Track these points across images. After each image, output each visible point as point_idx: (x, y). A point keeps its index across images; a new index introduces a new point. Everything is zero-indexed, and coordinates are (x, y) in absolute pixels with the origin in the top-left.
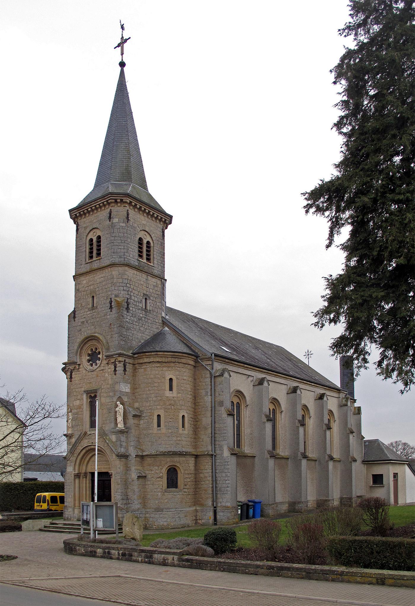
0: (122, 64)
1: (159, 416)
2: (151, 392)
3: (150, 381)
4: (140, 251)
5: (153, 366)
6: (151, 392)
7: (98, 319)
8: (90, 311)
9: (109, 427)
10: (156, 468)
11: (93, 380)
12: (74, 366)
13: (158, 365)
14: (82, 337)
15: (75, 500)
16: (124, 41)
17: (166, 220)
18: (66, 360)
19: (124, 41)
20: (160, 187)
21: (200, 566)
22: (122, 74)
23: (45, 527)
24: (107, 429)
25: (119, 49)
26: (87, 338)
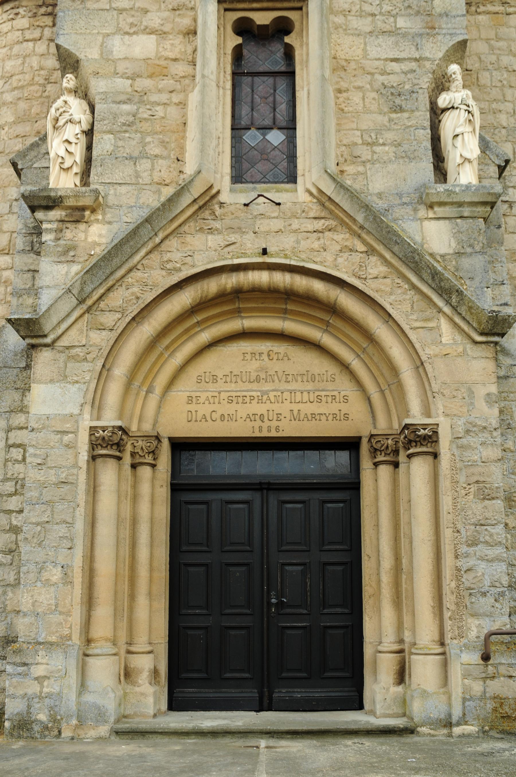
9: (391, 177)
15: (90, 601)
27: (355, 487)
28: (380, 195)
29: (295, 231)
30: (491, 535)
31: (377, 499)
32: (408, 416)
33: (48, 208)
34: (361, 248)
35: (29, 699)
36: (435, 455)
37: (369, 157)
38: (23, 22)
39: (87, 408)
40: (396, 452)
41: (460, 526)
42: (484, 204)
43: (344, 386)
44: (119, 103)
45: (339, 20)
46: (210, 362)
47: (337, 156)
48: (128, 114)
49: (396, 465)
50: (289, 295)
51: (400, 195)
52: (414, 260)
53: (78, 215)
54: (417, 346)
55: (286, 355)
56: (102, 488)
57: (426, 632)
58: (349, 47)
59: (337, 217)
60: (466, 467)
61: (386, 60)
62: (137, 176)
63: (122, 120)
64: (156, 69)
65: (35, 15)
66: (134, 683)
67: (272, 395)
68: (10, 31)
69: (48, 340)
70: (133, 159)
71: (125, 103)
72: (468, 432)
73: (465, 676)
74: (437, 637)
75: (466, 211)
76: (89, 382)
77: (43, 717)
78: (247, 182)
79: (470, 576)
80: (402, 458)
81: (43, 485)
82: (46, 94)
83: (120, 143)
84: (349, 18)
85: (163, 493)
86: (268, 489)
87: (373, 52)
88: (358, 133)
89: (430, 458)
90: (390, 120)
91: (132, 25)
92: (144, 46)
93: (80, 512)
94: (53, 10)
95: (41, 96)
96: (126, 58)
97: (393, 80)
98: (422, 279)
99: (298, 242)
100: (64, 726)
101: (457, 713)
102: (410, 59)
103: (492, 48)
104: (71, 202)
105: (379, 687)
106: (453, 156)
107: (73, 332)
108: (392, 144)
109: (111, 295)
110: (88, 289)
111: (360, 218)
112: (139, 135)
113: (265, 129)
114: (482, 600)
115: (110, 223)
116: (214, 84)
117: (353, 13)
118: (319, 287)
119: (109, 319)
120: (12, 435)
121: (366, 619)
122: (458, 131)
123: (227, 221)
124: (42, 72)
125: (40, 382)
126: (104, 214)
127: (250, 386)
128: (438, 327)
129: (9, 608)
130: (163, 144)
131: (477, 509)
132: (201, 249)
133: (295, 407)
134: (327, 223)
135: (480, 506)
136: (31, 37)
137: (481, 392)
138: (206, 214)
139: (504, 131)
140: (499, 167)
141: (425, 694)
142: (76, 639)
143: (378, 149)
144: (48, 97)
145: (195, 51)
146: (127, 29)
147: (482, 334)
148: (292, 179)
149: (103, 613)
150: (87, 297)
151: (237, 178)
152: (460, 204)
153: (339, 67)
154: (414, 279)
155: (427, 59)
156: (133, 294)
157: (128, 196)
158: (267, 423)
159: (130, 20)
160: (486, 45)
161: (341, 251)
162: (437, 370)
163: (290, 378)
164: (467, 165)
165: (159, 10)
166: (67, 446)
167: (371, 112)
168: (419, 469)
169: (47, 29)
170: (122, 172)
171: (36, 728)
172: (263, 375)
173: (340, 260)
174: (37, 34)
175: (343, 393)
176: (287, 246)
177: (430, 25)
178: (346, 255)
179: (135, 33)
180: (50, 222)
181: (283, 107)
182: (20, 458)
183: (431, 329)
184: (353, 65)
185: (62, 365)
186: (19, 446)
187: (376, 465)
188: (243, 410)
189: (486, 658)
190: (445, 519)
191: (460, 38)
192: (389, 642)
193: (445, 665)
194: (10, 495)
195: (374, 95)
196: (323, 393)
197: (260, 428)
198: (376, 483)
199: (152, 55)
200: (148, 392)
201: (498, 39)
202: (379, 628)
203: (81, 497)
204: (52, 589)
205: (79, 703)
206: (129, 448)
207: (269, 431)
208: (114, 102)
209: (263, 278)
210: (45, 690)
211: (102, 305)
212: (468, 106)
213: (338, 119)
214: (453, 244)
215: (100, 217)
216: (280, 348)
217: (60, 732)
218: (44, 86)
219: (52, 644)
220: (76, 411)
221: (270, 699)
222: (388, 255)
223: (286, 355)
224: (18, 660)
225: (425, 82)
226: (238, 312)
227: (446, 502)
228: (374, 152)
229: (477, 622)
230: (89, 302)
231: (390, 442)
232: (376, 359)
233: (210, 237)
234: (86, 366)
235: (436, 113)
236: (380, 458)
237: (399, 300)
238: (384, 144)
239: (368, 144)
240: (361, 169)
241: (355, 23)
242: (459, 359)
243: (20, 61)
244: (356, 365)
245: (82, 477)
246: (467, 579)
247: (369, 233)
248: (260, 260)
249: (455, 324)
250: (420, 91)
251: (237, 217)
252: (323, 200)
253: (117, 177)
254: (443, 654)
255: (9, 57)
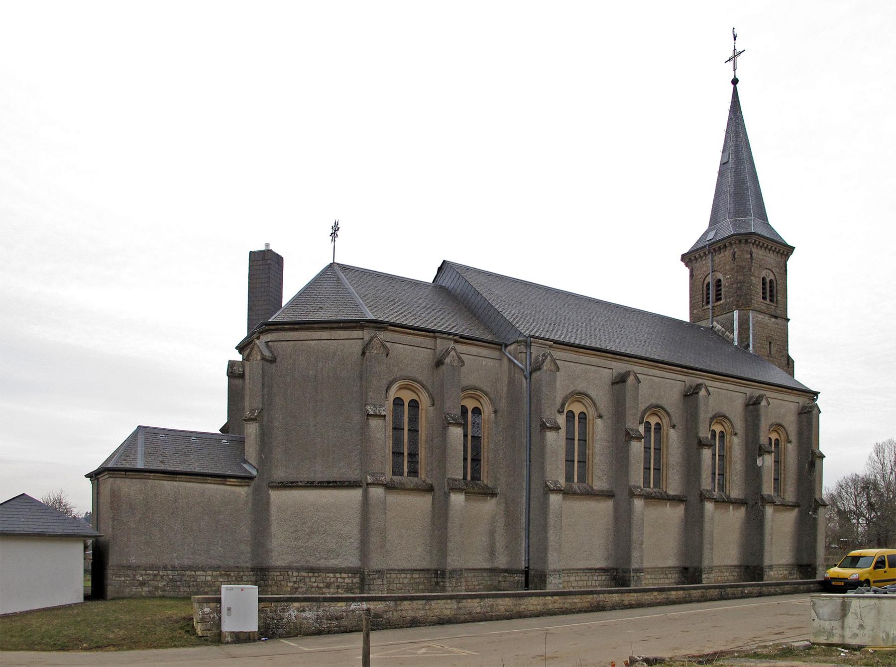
0: (735, 82)
4: (763, 293)
16: (736, 55)
17: (787, 251)
19: (736, 55)
20: (782, 219)
21: (599, 608)
22: (735, 91)
25: (731, 63)
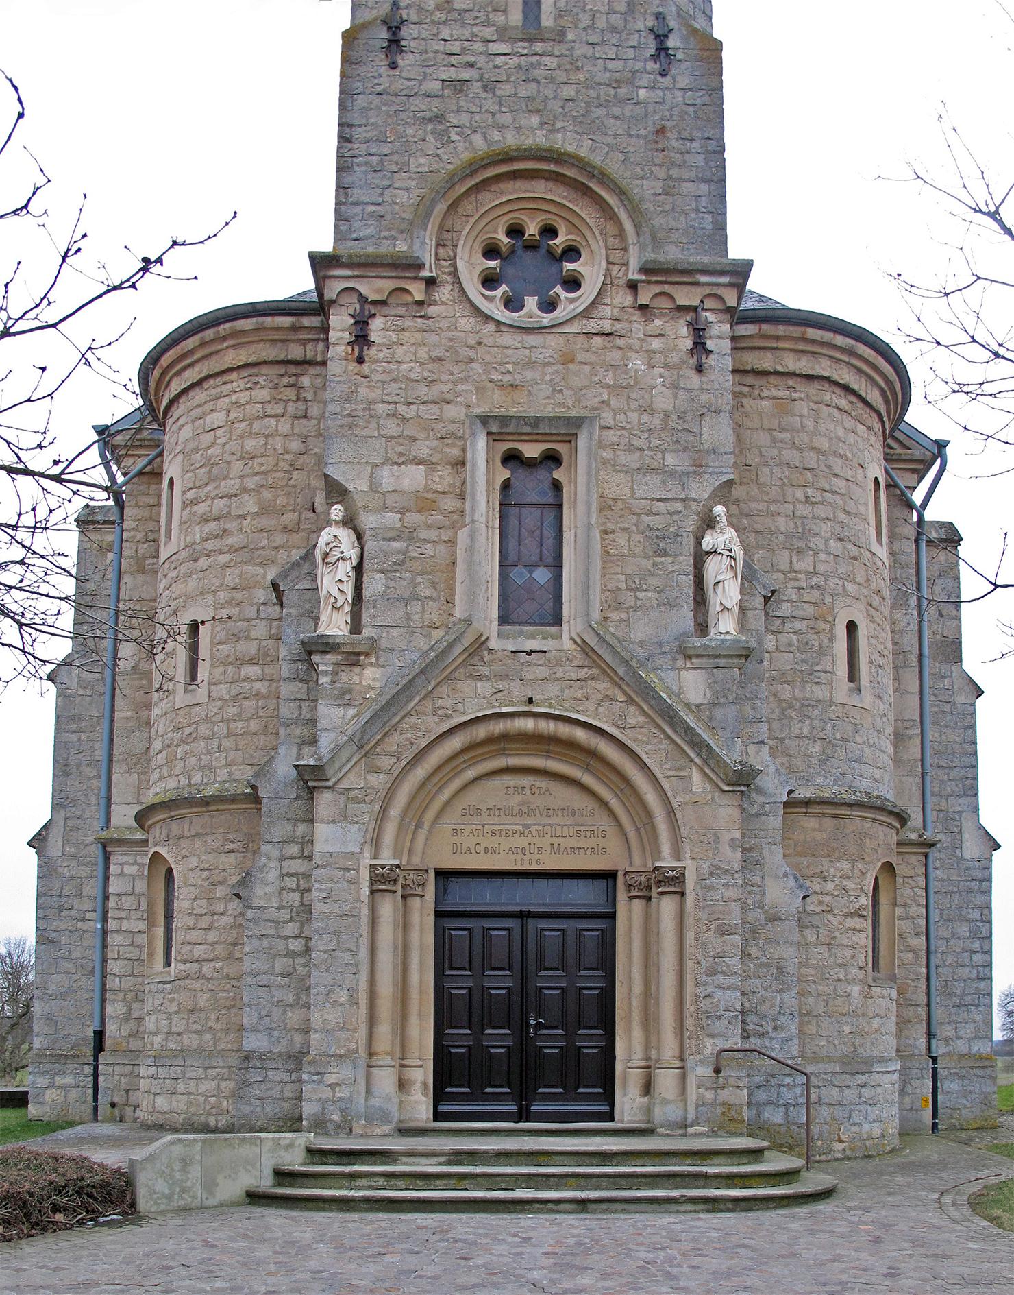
1: (851, 627)
2: (821, 511)
3: (812, 460)
5: (827, 397)
6: (821, 511)
7: (569, 91)
8: (513, 40)
9: (650, 627)
10: (846, 866)
11: (529, 375)
12: (389, 285)
13: (843, 403)
14: (461, 152)
15: (372, 1021)
18: (326, 244)
23: (283, 1176)
24: (640, 631)
26: (507, 157)
27: (612, 916)
28: (641, 644)
29: (559, 680)
30: (728, 966)
31: (630, 929)
32: (659, 859)
33: (325, 652)
34: (621, 697)
35: (323, 1103)
36: (683, 894)
37: (632, 604)
38: (262, 394)
39: (367, 847)
40: (649, 887)
41: (700, 958)
42: (740, 656)
43: (604, 823)
44: (389, 540)
45: (607, 455)
46: (473, 797)
47: (601, 602)
48: (398, 552)
49: (649, 899)
50: (553, 740)
51: (660, 644)
52: (667, 715)
53: (353, 659)
54: (669, 794)
55: (548, 790)
56: (382, 920)
57: (669, 1049)
58: (617, 485)
59: (600, 667)
60: (708, 905)
61: (653, 499)
62: (409, 619)
63: (392, 558)
64: (424, 502)
65: (276, 387)
66: (408, 1093)
67: (533, 828)
68: (248, 403)
69: (330, 783)
70: (404, 601)
71: (394, 540)
72: (711, 874)
73: (699, 1087)
74: (677, 1054)
75: (722, 662)
76: (368, 823)
77: (336, 1117)
78: (513, 623)
79: (708, 1001)
80: (654, 893)
81: (329, 917)
82: (291, 482)
83: (392, 584)
84: (618, 453)
85: (431, 920)
86: (528, 917)
87: (640, 493)
88: (623, 578)
89: (677, 897)
90: (655, 565)
91: (401, 454)
92: (413, 478)
93: (364, 941)
94: (297, 380)
95: (287, 485)
96: (395, 491)
97: (658, 522)
98: (676, 732)
99: (562, 691)
100: (354, 1125)
101: (691, 1116)
102: (676, 499)
103: (774, 440)
104: (348, 649)
105: (628, 1103)
106: (716, 601)
107: (352, 775)
108: (654, 590)
109: (387, 739)
110: (367, 736)
111: (621, 671)
112: (409, 575)
113: (532, 566)
114: (718, 1023)
115: (383, 666)
116: (483, 526)
117: (621, 447)
118: (580, 734)
119: (386, 763)
120: (286, 864)
121: (618, 1038)
122: (719, 578)
123: (496, 668)
124: (288, 457)
125: (322, 822)
126: (377, 658)
127: (512, 820)
128: (690, 776)
129: (289, 1026)
130: (434, 585)
131: (716, 943)
132: (473, 698)
133: (556, 841)
134: (590, 672)
135: (719, 941)
136: (273, 412)
137: (726, 837)
138: (476, 661)
139: (781, 537)
140: (765, 597)
141: (665, 1102)
142: (363, 1052)
143: (641, 595)
144: (294, 486)
145: (464, 483)
146: (396, 459)
147: (728, 785)
148: (558, 621)
149: (384, 1030)
150: (364, 745)
151: (504, 619)
152: (717, 657)
153: (606, 506)
154: (669, 731)
155: (693, 499)
156: (407, 739)
157: (401, 646)
158: (528, 856)
159: (399, 449)
160: (768, 436)
161: (602, 700)
162: (687, 818)
163: (551, 812)
164: (726, 612)
165: (427, 439)
166: (349, 882)
167: (636, 556)
168: (667, 907)
169: (290, 404)
170: (394, 615)
171: (331, 1126)
172: (525, 810)
173: (601, 710)
174: (279, 410)
175: (601, 828)
176: (552, 695)
177: (697, 462)
178: (606, 704)
179: (403, 463)
180: (326, 664)
181: (549, 542)
182: (294, 886)
183: (683, 778)
184: (620, 504)
185: (342, 806)
186: (292, 875)
187: (631, 898)
188: (505, 844)
189: (717, 1071)
190: (688, 951)
191: (727, 477)
192: (638, 1059)
193: (683, 1078)
194: (286, 922)
195: (639, 537)
196: (582, 828)
197: (522, 860)
198: (629, 915)
199: (421, 488)
200: (417, 827)
201: (782, 430)
202: (628, 1049)
203: (365, 929)
204: (340, 1009)
205: (366, 1107)
206: (401, 881)
207: (530, 863)
208: (384, 539)
209: (528, 725)
210: (338, 1095)
211: (378, 749)
212: (730, 551)
213: (604, 562)
214: (708, 695)
215: (373, 660)
216: (542, 783)
217: (351, 1130)
218: (290, 473)
219: (341, 1056)
220: (357, 850)
221: (528, 1109)
222: (646, 708)
223: (548, 790)
224: (312, 1069)
225: (691, 523)
226: (502, 752)
227: (690, 937)
228: (637, 598)
229: (712, 1041)
230: (367, 748)
231: (643, 878)
232: (632, 800)
233: (479, 684)
234: (365, 808)
235: (700, 558)
236: (634, 893)
237: (653, 751)
238: (647, 590)
239: (631, 590)
240: (624, 616)
241: (624, 458)
242: (707, 807)
243: (261, 441)
244: (614, 803)
245: (365, 911)
246: (706, 1005)
247: (628, 684)
248: (526, 709)
249: (705, 774)
250: (685, 534)
251: (504, 664)
252: (584, 647)
253: (389, 620)
254: (683, 1068)
255: (250, 435)
